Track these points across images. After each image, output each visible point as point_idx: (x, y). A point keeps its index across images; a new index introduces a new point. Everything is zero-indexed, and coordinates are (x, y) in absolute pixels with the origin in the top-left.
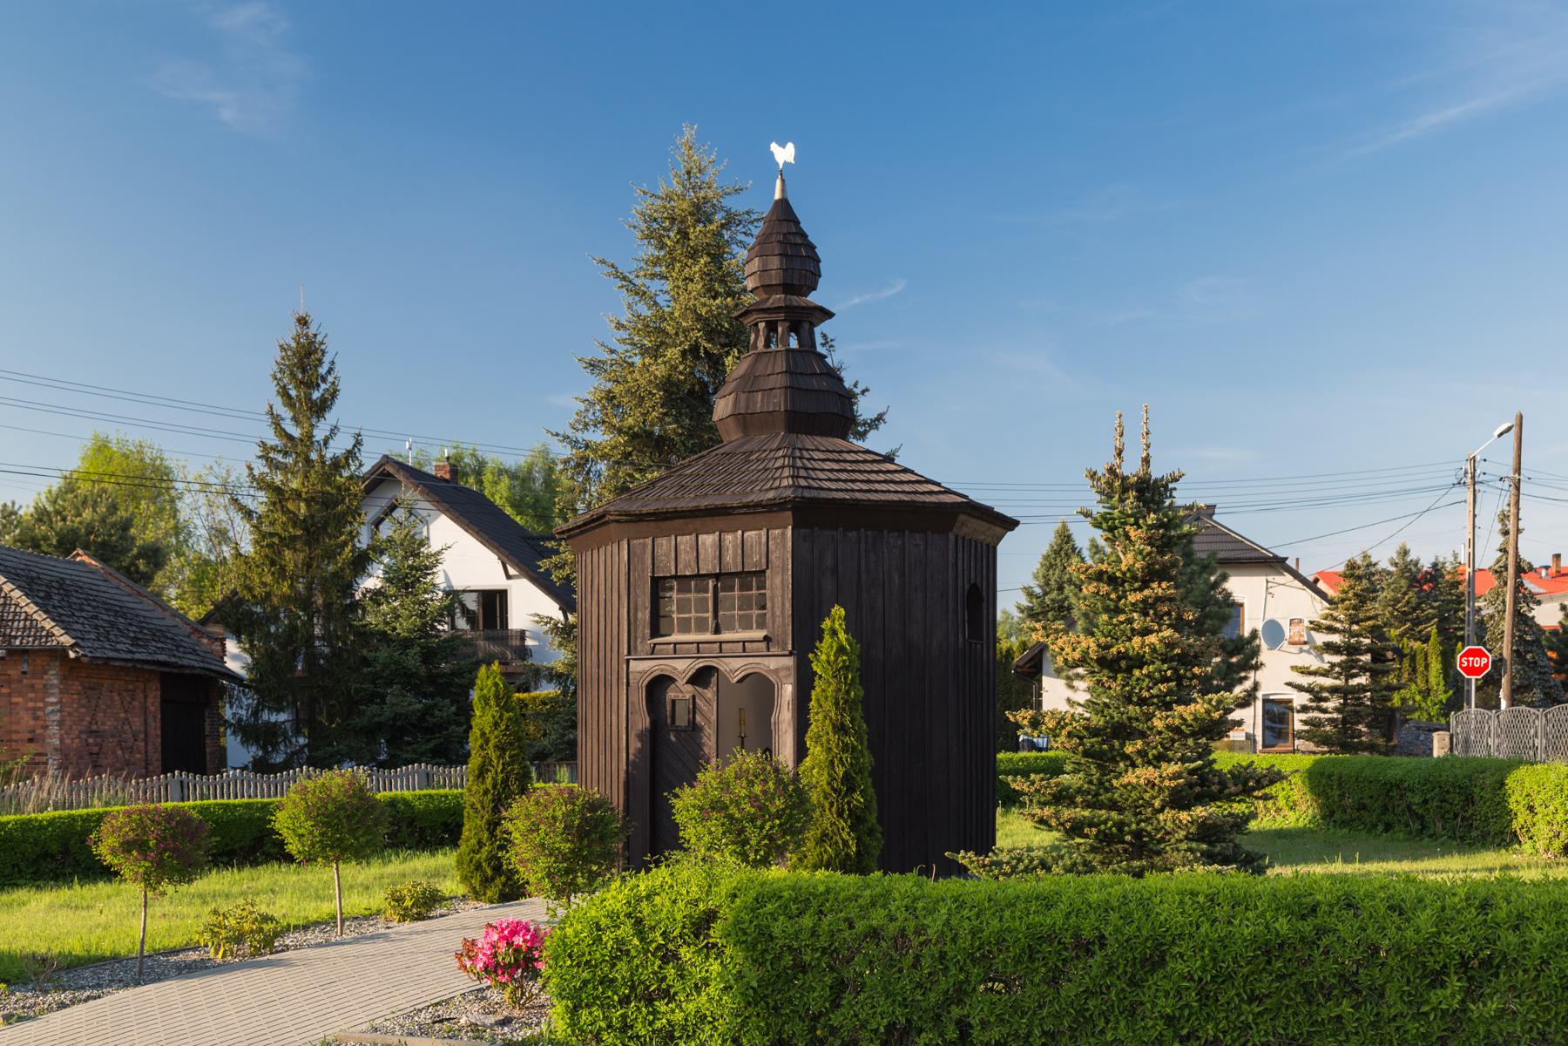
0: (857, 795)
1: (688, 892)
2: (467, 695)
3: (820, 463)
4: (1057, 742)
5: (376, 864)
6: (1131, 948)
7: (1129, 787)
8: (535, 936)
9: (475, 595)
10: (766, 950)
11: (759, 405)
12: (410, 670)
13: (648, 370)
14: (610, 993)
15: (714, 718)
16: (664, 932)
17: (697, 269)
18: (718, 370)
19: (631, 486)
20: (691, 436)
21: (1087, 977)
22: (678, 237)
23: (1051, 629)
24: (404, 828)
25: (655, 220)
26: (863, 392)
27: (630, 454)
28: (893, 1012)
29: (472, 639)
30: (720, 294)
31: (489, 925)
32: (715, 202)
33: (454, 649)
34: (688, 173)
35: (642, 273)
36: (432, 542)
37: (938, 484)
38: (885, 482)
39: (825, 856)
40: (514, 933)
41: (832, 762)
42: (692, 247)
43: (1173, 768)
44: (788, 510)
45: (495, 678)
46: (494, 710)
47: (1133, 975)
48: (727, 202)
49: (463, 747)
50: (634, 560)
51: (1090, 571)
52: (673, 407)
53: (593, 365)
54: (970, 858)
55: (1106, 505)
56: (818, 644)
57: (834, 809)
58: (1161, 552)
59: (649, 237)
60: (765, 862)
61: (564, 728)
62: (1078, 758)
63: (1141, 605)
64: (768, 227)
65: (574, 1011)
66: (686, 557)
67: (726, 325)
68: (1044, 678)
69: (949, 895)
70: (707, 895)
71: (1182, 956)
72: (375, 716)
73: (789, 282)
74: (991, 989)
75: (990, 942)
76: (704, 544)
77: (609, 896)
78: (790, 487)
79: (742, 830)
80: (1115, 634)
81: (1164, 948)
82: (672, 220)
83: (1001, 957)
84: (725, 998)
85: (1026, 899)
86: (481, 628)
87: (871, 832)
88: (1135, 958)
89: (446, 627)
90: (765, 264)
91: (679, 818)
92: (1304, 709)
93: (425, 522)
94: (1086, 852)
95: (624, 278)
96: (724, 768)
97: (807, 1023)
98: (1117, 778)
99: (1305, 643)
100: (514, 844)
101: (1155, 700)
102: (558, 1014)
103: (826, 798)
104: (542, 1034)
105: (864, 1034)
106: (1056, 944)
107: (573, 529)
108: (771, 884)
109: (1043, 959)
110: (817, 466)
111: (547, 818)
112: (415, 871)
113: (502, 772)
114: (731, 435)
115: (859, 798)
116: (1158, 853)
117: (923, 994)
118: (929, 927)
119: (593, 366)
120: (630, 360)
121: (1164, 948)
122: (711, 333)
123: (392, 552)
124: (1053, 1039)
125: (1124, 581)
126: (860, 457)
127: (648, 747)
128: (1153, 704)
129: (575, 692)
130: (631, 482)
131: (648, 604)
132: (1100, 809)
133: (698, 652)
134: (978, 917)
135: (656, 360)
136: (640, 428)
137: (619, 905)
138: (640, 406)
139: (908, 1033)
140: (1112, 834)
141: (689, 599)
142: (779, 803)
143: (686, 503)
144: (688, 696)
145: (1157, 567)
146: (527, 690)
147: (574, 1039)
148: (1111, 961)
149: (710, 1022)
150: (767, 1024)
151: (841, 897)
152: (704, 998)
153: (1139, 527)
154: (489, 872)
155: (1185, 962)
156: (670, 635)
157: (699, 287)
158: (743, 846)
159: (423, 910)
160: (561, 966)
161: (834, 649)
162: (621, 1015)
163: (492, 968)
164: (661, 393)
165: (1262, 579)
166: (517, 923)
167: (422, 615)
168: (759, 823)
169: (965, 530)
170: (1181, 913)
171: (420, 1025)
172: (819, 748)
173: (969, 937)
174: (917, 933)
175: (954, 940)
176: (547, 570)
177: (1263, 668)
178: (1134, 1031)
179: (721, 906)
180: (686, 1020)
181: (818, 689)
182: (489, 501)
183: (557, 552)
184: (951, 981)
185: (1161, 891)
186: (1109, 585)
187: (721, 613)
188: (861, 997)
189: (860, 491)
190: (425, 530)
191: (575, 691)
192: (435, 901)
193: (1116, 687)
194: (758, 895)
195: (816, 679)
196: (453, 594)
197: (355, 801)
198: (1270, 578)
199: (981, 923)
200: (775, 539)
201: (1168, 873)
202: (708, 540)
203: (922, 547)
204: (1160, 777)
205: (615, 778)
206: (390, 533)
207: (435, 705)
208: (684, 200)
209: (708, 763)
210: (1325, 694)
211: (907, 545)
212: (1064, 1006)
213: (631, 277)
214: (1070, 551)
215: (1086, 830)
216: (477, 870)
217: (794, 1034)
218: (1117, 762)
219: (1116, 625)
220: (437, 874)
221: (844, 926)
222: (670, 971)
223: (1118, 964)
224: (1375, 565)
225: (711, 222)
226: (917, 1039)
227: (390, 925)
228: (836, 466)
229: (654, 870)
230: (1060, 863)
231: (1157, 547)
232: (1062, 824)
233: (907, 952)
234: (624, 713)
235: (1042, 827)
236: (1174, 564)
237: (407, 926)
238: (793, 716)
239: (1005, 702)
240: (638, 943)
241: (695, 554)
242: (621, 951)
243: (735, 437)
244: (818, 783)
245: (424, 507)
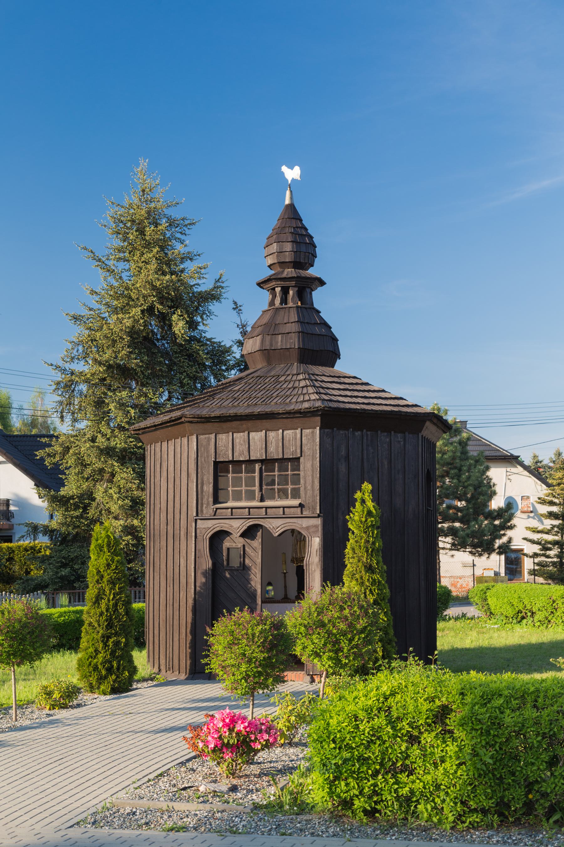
11: (279, 344)
13: (121, 323)
25: (122, 222)
27: (104, 379)
32: (160, 211)
34: (143, 191)
38: (376, 398)
44: (318, 416)
50: (201, 449)
52: (136, 348)
53: (76, 318)
56: (352, 509)
64: (282, 223)
65: (332, 784)
67: (173, 294)
73: (298, 260)
76: (254, 439)
82: (133, 221)
92: (535, 555)
95: (99, 260)
99: (531, 512)
113: (113, 599)
115: (384, 617)
122: (162, 299)
127: (210, 582)
131: (211, 480)
138: (113, 346)
143: (242, 410)
144: (240, 545)
154: (104, 672)
156: (227, 502)
161: (365, 513)
165: (504, 470)
172: (354, 582)
177: (515, 527)
183: (50, 445)
187: (264, 487)
197: (34, 621)
198: (508, 469)
200: (306, 436)
203: (402, 443)
210: (550, 546)
213: (104, 259)
224: (541, 462)
241: (247, 446)
242: (376, 734)
243: (260, 366)
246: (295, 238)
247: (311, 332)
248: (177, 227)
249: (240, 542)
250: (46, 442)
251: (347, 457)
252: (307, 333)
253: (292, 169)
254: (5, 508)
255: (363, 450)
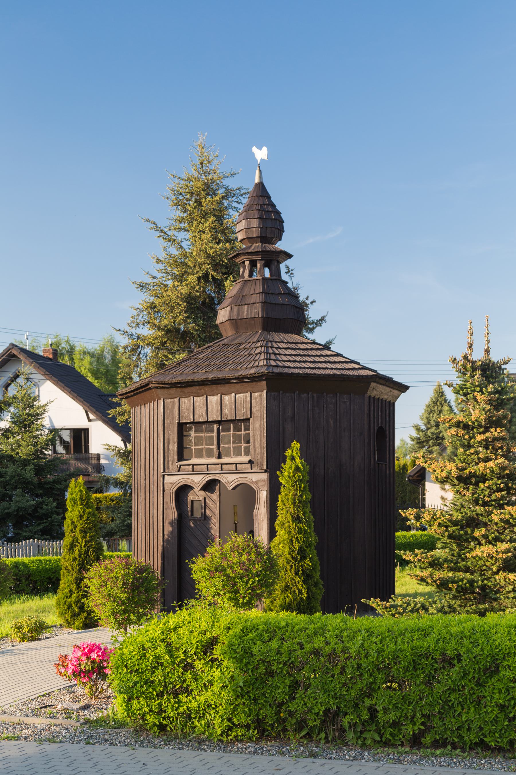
0: (307, 561)
1: (200, 626)
2: (64, 496)
3: (284, 350)
4: (431, 529)
5: (6, 604)
6: (478, 662)
7: (477, 558)
8: (104, 653)
9: (68, 431)
10: (249, 663)
11: (245, 314)
12: (27, 479)
13: (176, 290)
14: (151, 690)
15: (217, 512)
16: (185, 652)
17: (207, 225)
18: (220, 289)
19: (166, 363)
20: (204, 331)
21: (450, 680)
22: (195, 204)
23: (428, 457)
24: (24, 581)
25: (181, 194)
26: (312, 303)
27: (165, 342)
28: (328, 702)
29: (67, 460)
30: (222, 241)
31: (76, 646)
32: (218, 182)
33: (55, 466)
34: (202, 163)
35: (173, 228)
36: (41, 398)
37: (358, 363)
38: (325, 362)
39: (288, 600)
40: (91, 651)
41: (291, 540)
42: (204, 211)
43: (504, 546)
45: (80, 487)
46: (79, 507)
47: (479, 679)
48: (226, 182)
49: (61, 528)
50: (167, 412)
51: (452, 421)
52: (192, 313)
53: (142, 286)
54: (377, 603)
55: (462, 379)
56: (283, 465)
57: (293, 570)
58: (497, 409)
59: (177, 205)
60: (249, 605)
61: (125, 517)
62: (445, 539)
63: (484, 443)
64: (251, 201)
66: (200, 410)
67: (226, 261)
68: (427, 484)
69: (363, 628)
70: (212, 628)
71: (509, 667)
72: (6, 509)
73: (264, 235)
74: (390, 688)
75: (389, 658)
76: (211, 402)
77: (150, 628)
78: (265, 366)
79: (235, 584)
80: (468, 461)
81: (498, 662)
82: (192, 194)
83: (396, 667)
84: (223, 693)
85: (411, 631)
86: (72, 452)
87: (316, 585)
88: (480, 668)
89: (50, 452)
90: (249, 224)
91: (195, 577)
93: (37, 385)
94: (450, 599)
95: (162, 231)
96: (223, 545)
97: (274, 709)
98: (469, 552)
100: (91, 594)
101: (493, 503)
102: (119, 703)
103: (288, 563)
104: (109, 715)
105: (311, 716)
106: (430, 659)
107: (129, 392)
108: (252, 621)
109: (422, 669)
110: (282, 352)
111: (112, 578)
112: (30, 609)
113: (84, 546)
114: (228, 332)
116: (496, 600)
117: (347, 691)
118: (350, 648)
119: (142, 286)
120: (165, 283)
121: (498, 662)
122: (216, 266)
123: (16, 405)
124: (429, 719)
125: (473, 428)
126: (309, 346)
127: (176, 530)
128: (492, 505)
129: (131, 494)
130: (166, 361)
131: (176, 440)
132: (459, 572)
133: (208, 470)
134: (381, 641)
135: (181, 283)
136: (172, 326)
137: (157, 634)
138: (172, 312)
139: (338, 715)
140: (466, 588)
141: (202, 437)
142: (258, 567)
143: (199, 376)
144: (201, 498)
145: (494, 418)
146: (101, 492)
147: (129, 719)
148: (465, 670)
149: (214, 708)
150: (249, 709)
151: (296, 628)
152: (210, 693)
153: (483, 393)
154: (77, 610)
155: (511, 670)
156: (190, 459)
157: (209, 236)
158: (236, 594)
159: (35, 635)
160: (120, 673)
161: (293, 468)
162: (158, 704)
163: (78, 673)
164: (185, 304)
166: (93, 644)
167: (35, 444)
168: (245, 579)
169: (375, 392)
170: (509, 640)
171: (32, 709)
172: (283, 531)
173: (376, 655)
174: (343, 652)
175: (366, 657)
176: (114, 416)
178: (480, 715)
179: (220, 635)
180: (199, 707)
181: (283, 494)
182: (77, 371)
183: (120, 405)
184: (365, 682)
185: (497, 625)
186: (464, 430)
187: (222, 446)
188: (309, 692)
189: (309, 368)
190: (37, 390)
191: (131, 492)
192: (42, 629)
193: (469, 495)
194: (244, 627)
195: (282, 487)
196: (54, 431)
199: (383, 646)
200: (255, 398)
201: (502, 612)
202: (214, 400)
203: (348, 403)
204: (497, 552)
205: (155, 550)
206: (15, 393)
207: (43, 502)
208: (199, 181)
209: (213, 542)
211: (338, 403)
212: (435, 698)
213: (166, 230)
214: (443, 402)
215: (450, 585)
216: (69, 608)
217: (266, 716)
218: (470, 542)
219: (468, 455)
220: (43, 610)
221: (297, 647)
222: (189, 676)
223: (470, 672)
225: (216, 195)
226: (343, 719)
227: (14, 644)
228: (293, 352)
229: (179, 612)
230: (434, 606)
231: (494, 406)
232: (435, 582)
233: (337, 663)
234: (162, 509)
235: (423, 583)
236: (505, 417)
237: (26, 645)
238: (267, 511)
239: (402, 498)
240: (168, 658)
241: (205, 408)
242: (158, 664)
243: (231, 334)
244: (283, 553)
245: (36, 375)
246: (262, 215)
247: (274, 302)
248: (233, 197)
249: (202, 494)
250: (117, 402)
251: (293, 418)
252: (271, 304)
253: (261, 150)
254: (96, 462)
255: (308, 412)
